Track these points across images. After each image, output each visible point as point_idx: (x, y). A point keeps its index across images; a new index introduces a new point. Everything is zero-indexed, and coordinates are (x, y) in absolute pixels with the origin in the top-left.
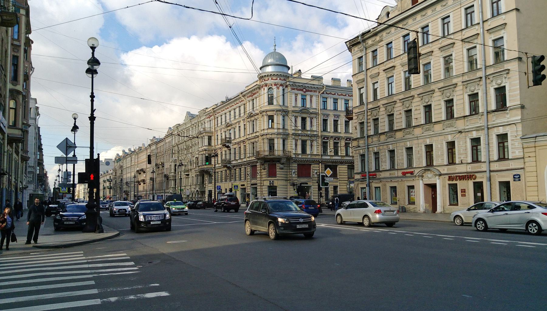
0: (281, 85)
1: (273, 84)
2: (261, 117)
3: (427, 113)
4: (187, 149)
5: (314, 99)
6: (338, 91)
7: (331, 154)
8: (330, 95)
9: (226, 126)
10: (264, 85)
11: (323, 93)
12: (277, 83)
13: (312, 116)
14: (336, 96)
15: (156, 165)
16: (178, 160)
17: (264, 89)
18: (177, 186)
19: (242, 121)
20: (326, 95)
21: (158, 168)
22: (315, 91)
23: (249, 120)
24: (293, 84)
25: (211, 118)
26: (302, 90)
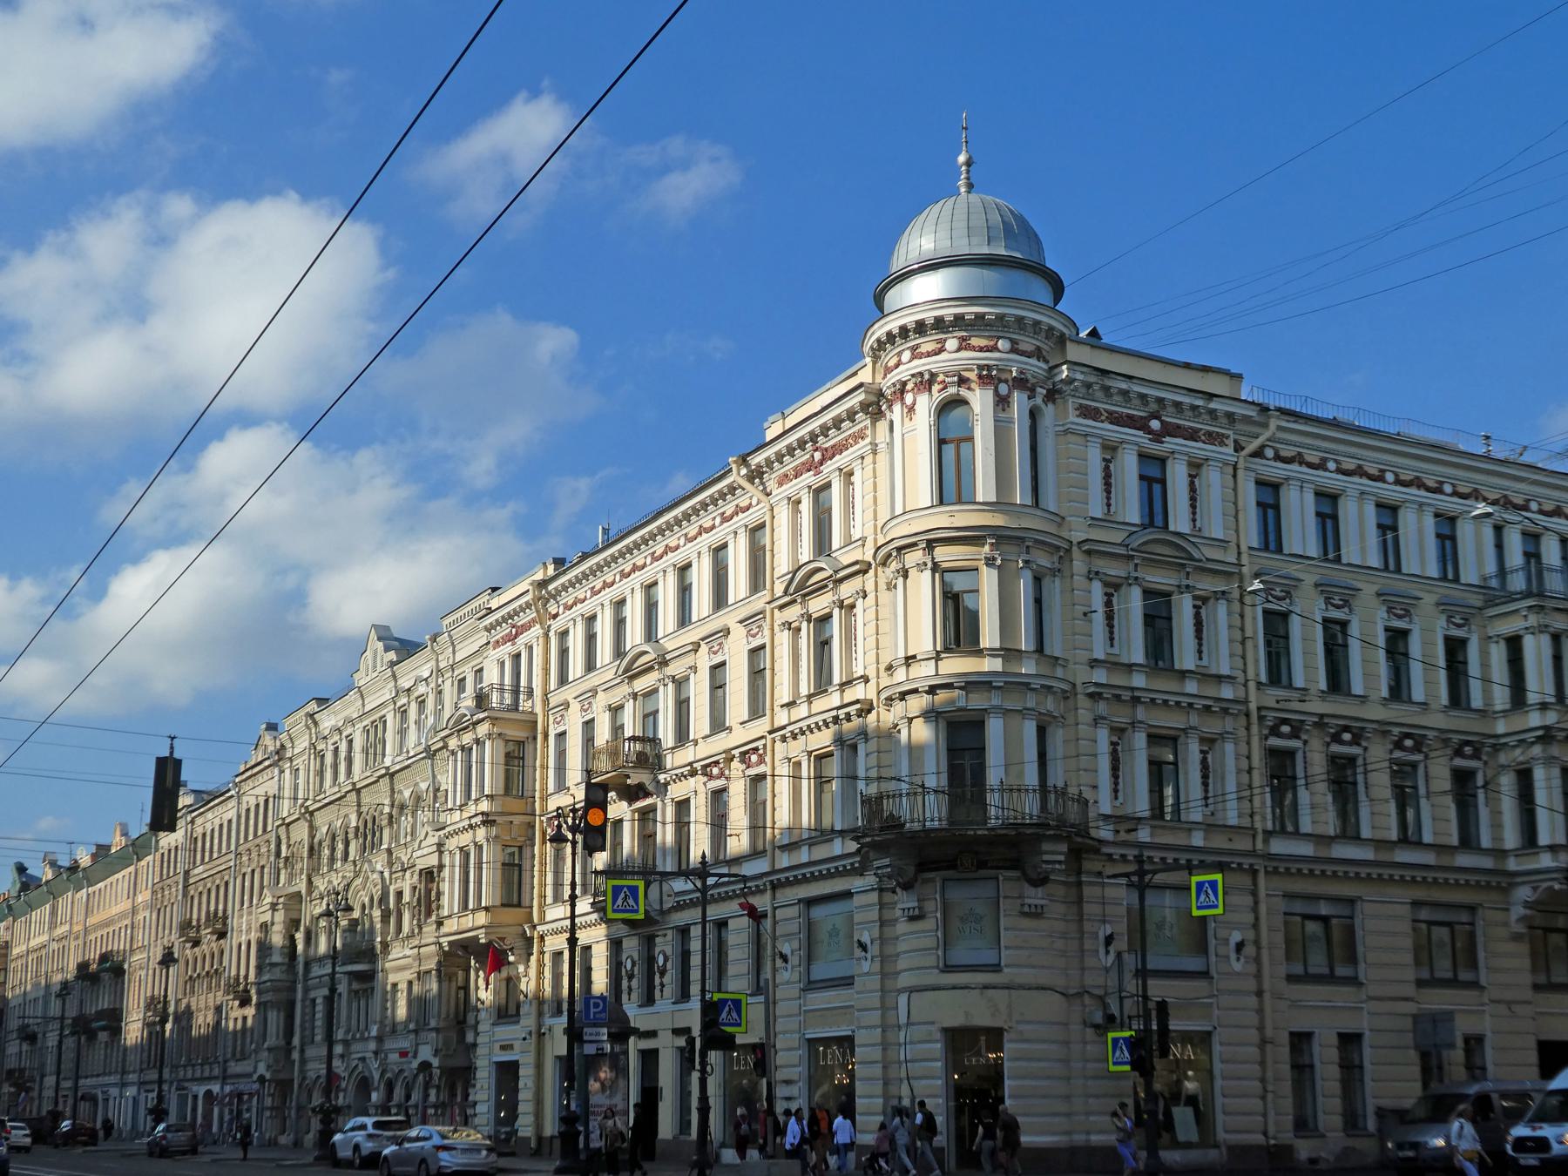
0: (1021, 383)
1: (972, 375)
2: (882, 586)
3: (461, 1018)
4: (369, 833)
5: (1213, 479)
6: (1342, 448)
7: (1320, 830)
8: (1295, 467)
9: (626, 671)
10: (909, 386)
11: (1258, 454)
12: (999, 370)
13: (1207, 585)
14: (1327, 474)
15: (185, 926)
16: (310, 892)
17: (911, 409)
18: (296, 1041)
19: (738, 632)
20: (1272, 463)
21: (193, 947)
22: (1214, 438)
23: (793, 613)
24: (1092, 379)
25: (522, 640)
26: (1140, 424)
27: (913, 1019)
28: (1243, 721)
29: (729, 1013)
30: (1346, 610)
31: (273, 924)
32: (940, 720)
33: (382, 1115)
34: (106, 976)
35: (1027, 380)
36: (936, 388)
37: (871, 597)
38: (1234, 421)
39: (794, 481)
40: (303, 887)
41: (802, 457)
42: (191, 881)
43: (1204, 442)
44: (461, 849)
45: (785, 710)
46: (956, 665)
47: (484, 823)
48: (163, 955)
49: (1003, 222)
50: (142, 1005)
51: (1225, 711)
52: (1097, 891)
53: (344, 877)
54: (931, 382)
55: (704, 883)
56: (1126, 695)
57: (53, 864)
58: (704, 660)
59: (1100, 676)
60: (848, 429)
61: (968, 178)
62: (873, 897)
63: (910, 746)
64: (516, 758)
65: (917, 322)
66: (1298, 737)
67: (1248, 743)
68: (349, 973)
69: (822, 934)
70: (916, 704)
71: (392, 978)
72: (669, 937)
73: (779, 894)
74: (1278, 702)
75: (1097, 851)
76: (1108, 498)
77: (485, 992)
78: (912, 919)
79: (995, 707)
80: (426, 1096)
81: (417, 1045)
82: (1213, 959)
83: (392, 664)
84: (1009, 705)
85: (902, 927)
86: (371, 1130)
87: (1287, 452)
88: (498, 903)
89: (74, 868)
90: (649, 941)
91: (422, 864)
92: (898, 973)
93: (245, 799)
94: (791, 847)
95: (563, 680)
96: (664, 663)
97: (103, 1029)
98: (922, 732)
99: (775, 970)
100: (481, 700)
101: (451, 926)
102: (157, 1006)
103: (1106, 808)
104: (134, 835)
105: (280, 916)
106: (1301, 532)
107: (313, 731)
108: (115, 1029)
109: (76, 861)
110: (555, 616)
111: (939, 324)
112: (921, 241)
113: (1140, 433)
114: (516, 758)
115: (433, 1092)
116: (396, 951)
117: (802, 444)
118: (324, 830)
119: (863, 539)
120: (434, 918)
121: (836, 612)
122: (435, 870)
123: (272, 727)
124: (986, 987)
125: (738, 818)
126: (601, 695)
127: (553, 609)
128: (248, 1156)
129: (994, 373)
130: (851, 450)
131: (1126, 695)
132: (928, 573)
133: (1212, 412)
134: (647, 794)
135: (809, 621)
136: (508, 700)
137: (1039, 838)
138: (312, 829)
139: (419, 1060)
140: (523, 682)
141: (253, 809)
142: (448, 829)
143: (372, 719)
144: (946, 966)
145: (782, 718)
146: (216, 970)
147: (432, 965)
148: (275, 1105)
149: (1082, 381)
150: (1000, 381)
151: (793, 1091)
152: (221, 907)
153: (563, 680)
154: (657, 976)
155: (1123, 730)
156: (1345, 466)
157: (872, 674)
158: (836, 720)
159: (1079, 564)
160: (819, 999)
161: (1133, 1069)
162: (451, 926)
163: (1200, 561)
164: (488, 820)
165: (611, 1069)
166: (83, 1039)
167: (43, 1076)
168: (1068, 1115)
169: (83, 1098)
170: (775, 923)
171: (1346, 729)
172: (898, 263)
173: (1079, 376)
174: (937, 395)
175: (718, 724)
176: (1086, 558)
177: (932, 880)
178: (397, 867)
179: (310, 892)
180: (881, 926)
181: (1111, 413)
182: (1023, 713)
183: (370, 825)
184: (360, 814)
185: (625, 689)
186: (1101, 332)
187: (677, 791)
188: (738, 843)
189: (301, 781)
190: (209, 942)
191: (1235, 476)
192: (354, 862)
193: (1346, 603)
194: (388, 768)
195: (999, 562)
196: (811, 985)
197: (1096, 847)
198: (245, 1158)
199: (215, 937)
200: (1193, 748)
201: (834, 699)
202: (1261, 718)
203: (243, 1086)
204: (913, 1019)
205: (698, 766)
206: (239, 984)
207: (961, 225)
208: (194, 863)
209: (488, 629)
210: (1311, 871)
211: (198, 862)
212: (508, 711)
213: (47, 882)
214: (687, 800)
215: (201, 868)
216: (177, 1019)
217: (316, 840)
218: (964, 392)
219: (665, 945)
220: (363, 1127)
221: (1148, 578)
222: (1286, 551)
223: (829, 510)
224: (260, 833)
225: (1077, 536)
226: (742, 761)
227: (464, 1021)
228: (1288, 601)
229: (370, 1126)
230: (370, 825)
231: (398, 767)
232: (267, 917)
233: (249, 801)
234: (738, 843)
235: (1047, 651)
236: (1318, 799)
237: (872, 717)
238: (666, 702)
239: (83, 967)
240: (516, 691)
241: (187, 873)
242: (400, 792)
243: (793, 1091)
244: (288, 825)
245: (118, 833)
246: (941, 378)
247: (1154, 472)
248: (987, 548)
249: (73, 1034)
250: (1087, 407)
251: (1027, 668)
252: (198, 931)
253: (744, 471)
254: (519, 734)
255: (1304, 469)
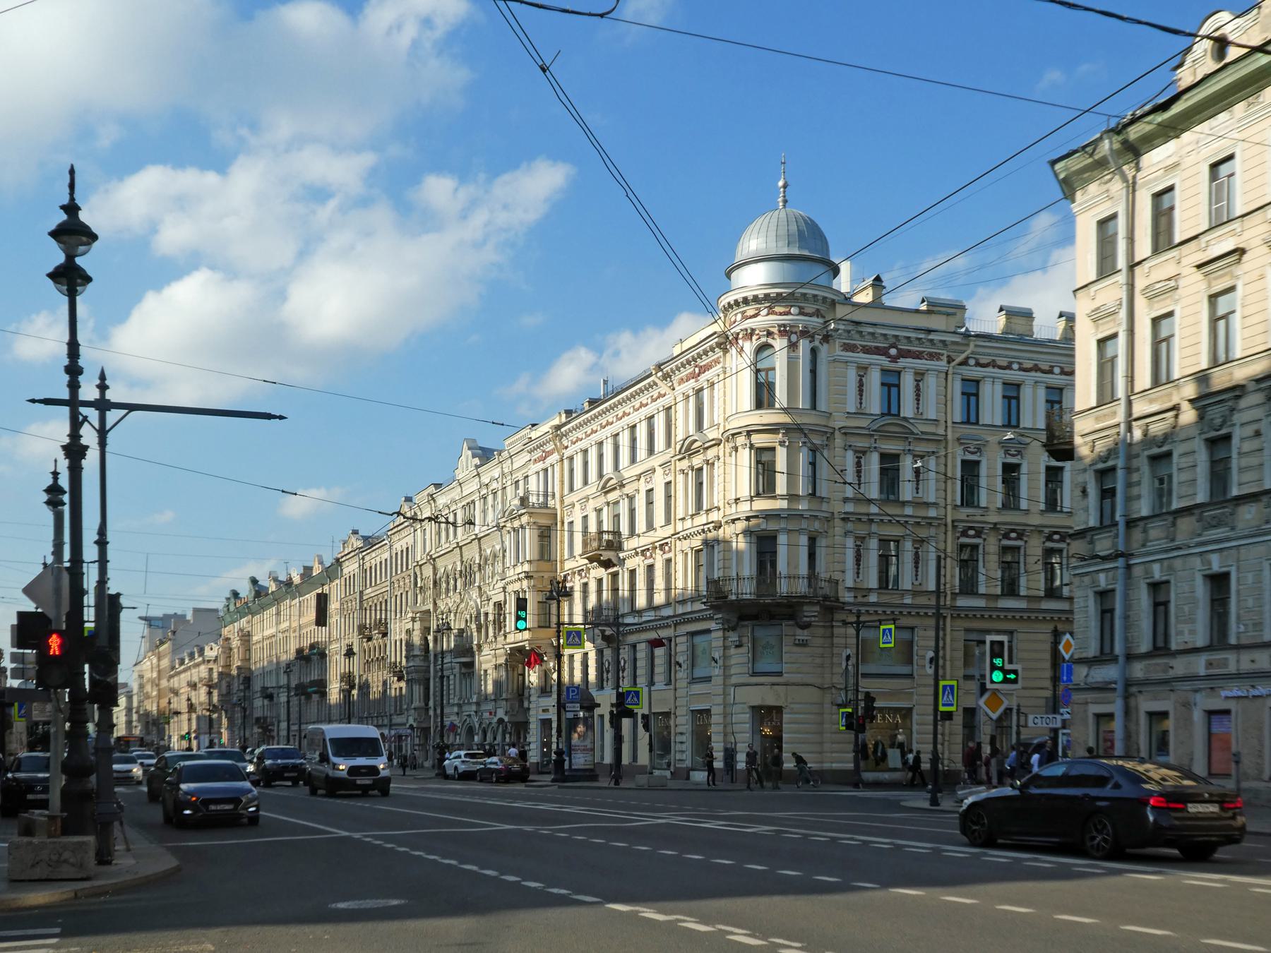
0: (805, 333)
1: (775, 330)
3: (521, 693)
4: (467, 574)
5: (931, 383)
8: (990, 369)
9: (604, 487)
10: (740, 336)
11: (964, 363)
12: (791, 326)
16: (435, 610)
19: (659, 471)
21: (368, 641)
22: (932, 356)
24: (850, 328)
26: (883, 352)
27: (736, 702)
28: (943, 528)
29: (632, 698)
30: (1019, 457)
31: (413, 630)
32: (753, 536)
33: (469, 750)
34: (315, 658)
35: (809, 332)
36: (755, 337)
37: (722, 460)
38: (946, 345)
39: (686, 384)
40: (431, 607)
41: (689, 370)
42: (365, 598)
43: (926, 359)
44: (515, 592)
45: (681, 522)
46: (762, 505)
47: (526, 577)
48: (347, 650)
49: (798, 230)
50: (339, 677)
51: (930, 524)
52: (842, 630)
53: (455, 602)
54: (751, 335)
55: (618, 629)
56: (865, 518)
57: (275, 579)
58: (643, 486)
59: (850, 508)
60: (712, 357)
61: (784, 196)
62: (720, 634)
63: (737, 551)
64: (546, 535)
65: (754, 296)
66: (980, 537)
67: (945, 542)
68: (459, 663)
69: (699, 652)
70: (741, 526)
71: (484, 666)
72: (627, 650)
73: (678, 627)
74: (968, 516)
75: (843, 609)
76: (861, 399)
77: (533, 677)
78: (737, 647)
79: (782, 529)
80: (504, 738)
81: (496, 708)
82: (915, 666)
83: (477, 467)
84: (791, 527)
85: (733, 651)
86: (463, 759)
87: (984, 360)
88: (536, 626)
89: (289, 583)
90: (617, 652)
91: (495, 599)
92: (731, 675)
93: (394, 547)
94: (683, 602)
95: (571, 490)
96: (622, 486)
97: (315, 692)
98: (741, 544)
99: (676, 672)
100: (524, 501)
101: (511, 638)
102: (348, 679)
103: (850, 583)
104: (327, 564)
105: (417, 625)
106: (992, 407)
107: (433, 505)
108: (323, 694)
109: (291, 579)
110: (567, 447)
111: (756, 299)
112: (753, 243)
113: (883, 358)
114: (546, 535)
115: (507, 736)
116: (486, 650)
117: (689, 362)
118: (442, 570)
119: (719, 425)
120: (502, 632)
121: (705, 466)
122: (502, 603)
123: (408, 499)
124: (773, 684)
125: (659, 583)
126: (591, 501)
127: (565, 443)
128: (406, 773)
129: (788, 329)
130: (713, 369)
131: (865, 518)
132: (748, 450)
133: (932, 341)
134: (614, 565)
135: (692, 470)
136: (541, 499)
137: (803, 604)
138: (435, 568)
139: (497, 717)
140: (550, 490)
141: (399, 553)
142: (506, 580)
143: (467, 501)
144: (753, 673)
145: (679, 527)
146: (383, 657)
147: (502, 660)
148: (421, 742)
149: (844, 330)
150: (792, 333)
151: (683, 738)
152: (383, 617)
153: (571, 490)
154: (621, 672)
155: (864, 538)
156: (1025, 366)
157: (722, 507)
158: (703, 531)
159: (839, 440)
160: (697, 688)
161: (847, 729)
162: (511, 638)
163: (918, 434)
164: (528, 576)
165: (584, 725)
166: (303, 697)
167: (279, 722)
168: (820, 753)
169: (1073, 557)
170: (676, 645)
171: (1013, 531)
172: (739, 257)
173: (843, 327)
174: (755, 342)
175: (650, 526)
176: (844, 437)
177: (747, 626)
178: (484, 598)
179: (435, 610)
180: (724, 649)
181: (864, 347)
182: (799, 531)
183: (468, 570)
184: (462, 562)
185: (602, 500)
186: (883, 278)
187: (630, 564)
188: (659, 598)
189: (428, 537)
190: (377, 640)
191: (946, 379)
192: (460, 593)
193: (1019, 453)
194: (476, 535)
195: (787, 444)
196: (694, 680)
197: (842, 607)
198: (404, 775)
199: (381, 636)
200: (908, 545)
201: (702, 519)
202: (954, 527)
203: (403, 731)
204: (736, 702)
205: (639, 550)
206: (396, 667)
207: (772, 234)
208: (366, 586)
209: (530, 452)
210: (982, 616)
211: (368, 586)
212: (540, 508)
213: (273, 592)
214: (635, 570)
215: (370, 590)
216: (360, 688)
217: (438, 577)
218: (770, 341)
219: (625, 654)
220: (459, 757)
221: (883, 446)
222: (981, 423)
223: (703, 403)
224: (404, 569)
225: (838, 424)
226: (661, 550)
227: (523, 695)
228: (978, 454)
229: (463, 757)
230: (468, 570)
231: (482, 535)
232: (410, 626)
233: (398, 547)
234: (659, 598)
235: (818, 494)
236: (992, 574)
237: (721, 531)
238: (624, 509)
239: (300, 651)
240: (546, 495)
241: (361, 593)
242: (485, 550)
243: (683, 738)
244: (421, 566)
245: (317, 563)
246: (757, 332)
247: (893, 380)
248: (781, 435)
249: (296, 695)
250: (848, 344)
251: (802, 506)
252: (371, 632)
253: (660, 374)
254: (544, 521)
255: (996, 370)
